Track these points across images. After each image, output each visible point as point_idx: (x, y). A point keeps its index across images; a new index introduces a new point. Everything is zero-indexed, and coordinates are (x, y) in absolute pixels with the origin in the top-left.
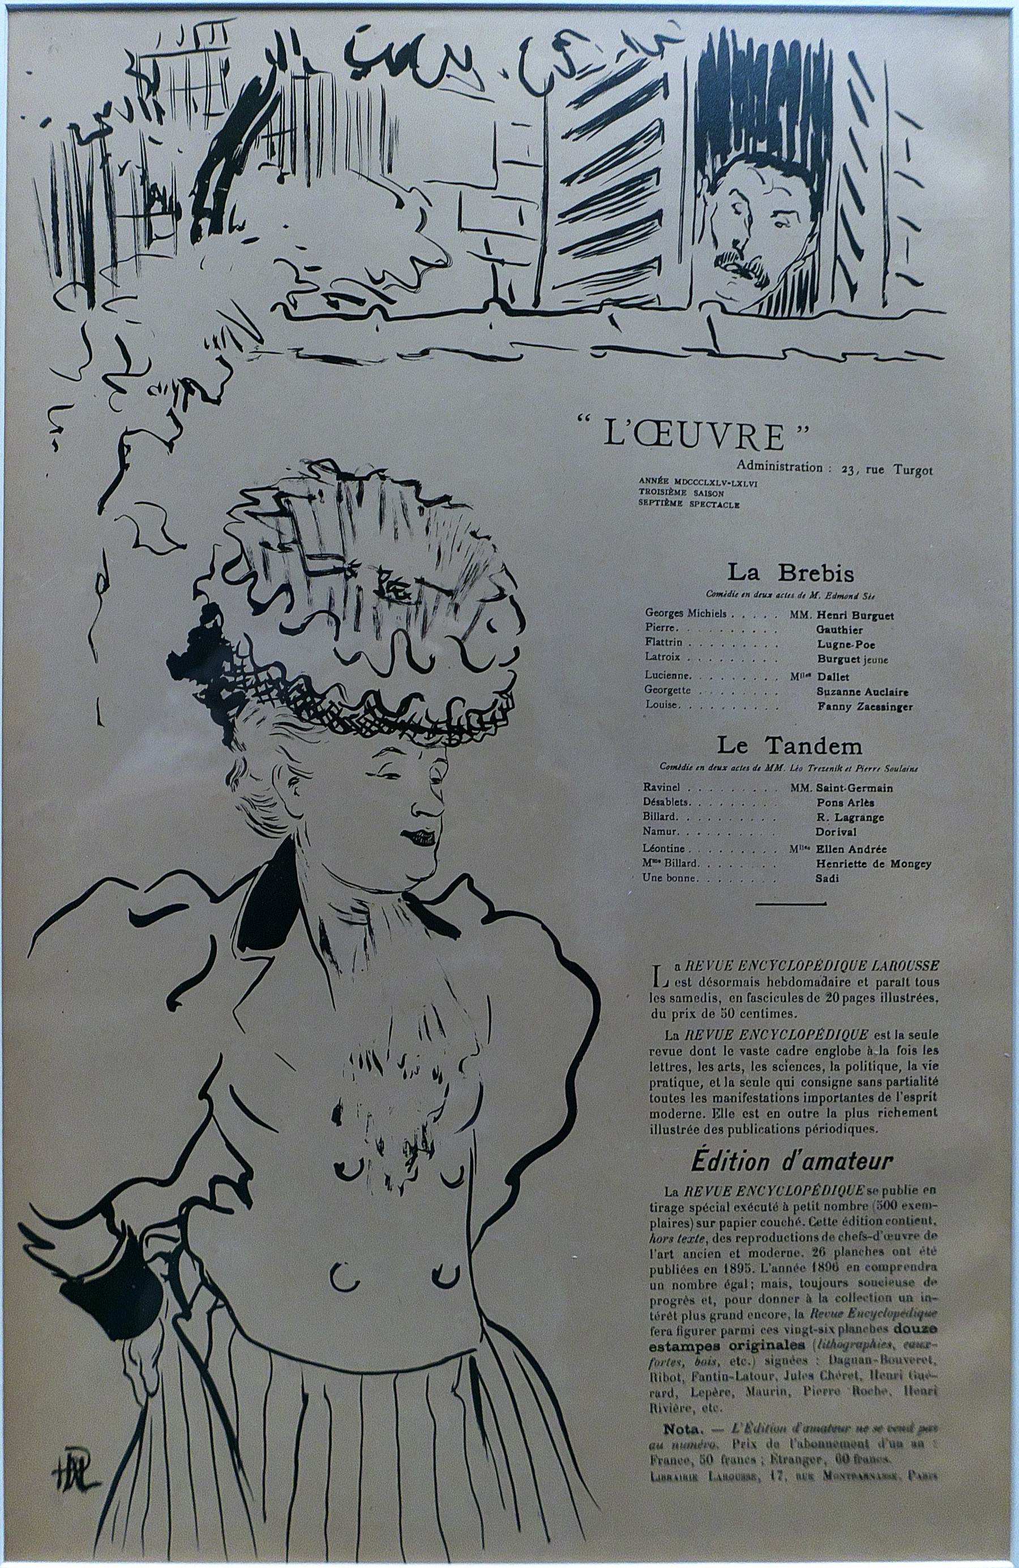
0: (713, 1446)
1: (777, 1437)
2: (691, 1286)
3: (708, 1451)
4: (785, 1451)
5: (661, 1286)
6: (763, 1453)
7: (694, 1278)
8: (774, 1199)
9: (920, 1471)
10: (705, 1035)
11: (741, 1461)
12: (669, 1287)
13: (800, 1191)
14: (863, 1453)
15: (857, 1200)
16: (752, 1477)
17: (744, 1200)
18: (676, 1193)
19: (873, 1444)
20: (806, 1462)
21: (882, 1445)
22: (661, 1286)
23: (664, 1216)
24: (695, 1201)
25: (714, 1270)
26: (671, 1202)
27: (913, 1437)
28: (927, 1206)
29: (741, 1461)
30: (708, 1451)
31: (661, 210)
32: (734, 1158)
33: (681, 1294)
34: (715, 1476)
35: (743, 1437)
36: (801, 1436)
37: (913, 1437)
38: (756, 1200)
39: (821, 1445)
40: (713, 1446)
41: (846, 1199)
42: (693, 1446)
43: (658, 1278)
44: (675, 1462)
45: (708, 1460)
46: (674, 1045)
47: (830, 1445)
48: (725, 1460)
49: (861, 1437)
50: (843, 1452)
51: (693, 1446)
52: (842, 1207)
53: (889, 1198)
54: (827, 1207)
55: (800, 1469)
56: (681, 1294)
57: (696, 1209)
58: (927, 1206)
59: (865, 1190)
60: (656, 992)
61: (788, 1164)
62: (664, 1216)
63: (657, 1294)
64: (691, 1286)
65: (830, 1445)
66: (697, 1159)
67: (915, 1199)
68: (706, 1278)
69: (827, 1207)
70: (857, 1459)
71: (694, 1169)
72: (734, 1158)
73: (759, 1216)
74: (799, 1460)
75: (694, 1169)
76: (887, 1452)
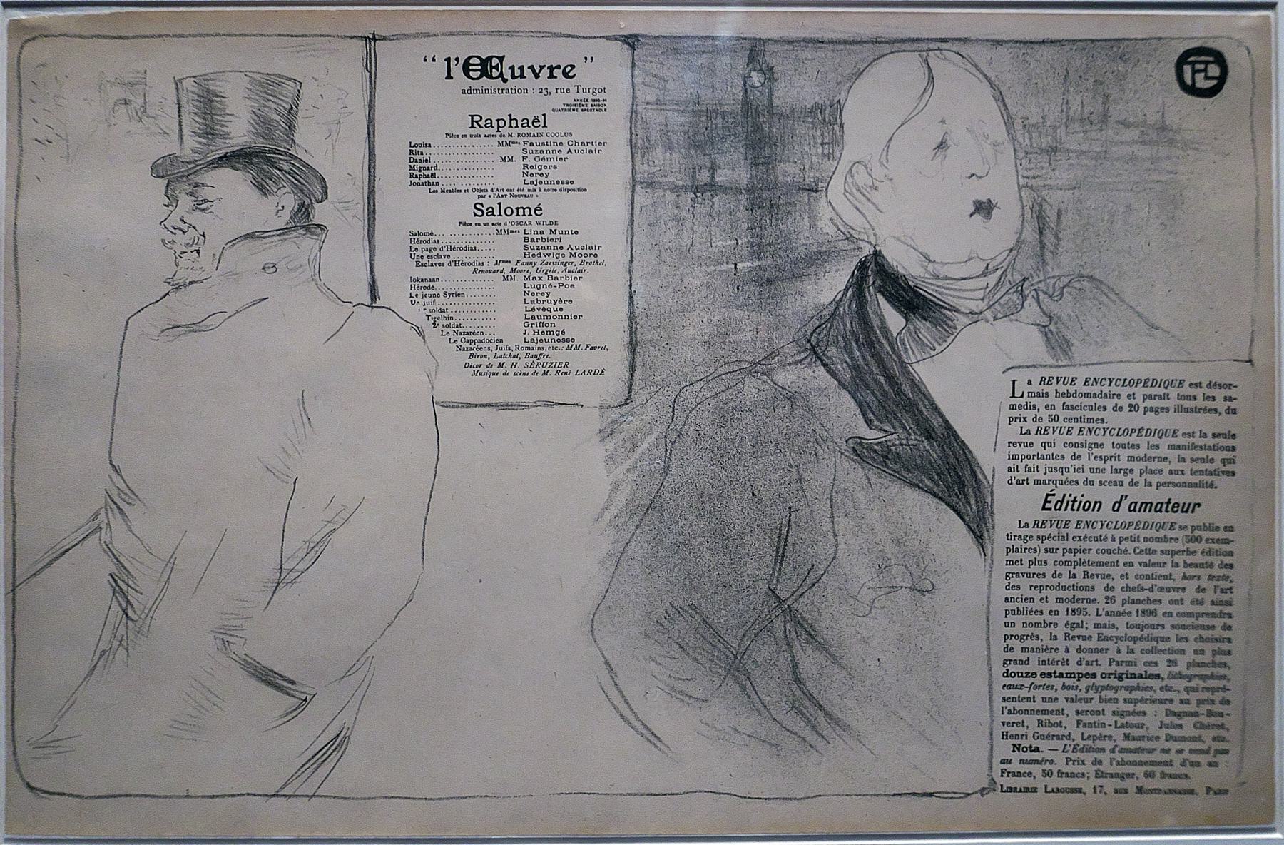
0: (1052, 762)
1: (1100, 756)
2: (1037, 625)
3: (1047, 767)
4: (1105, 767)
5: (1013, 625)
6: (1089, 769)
7: (1039, 619)
8: (1104, 532)
9: (1215, 787)
10: (1048, 524)
11: (1073, 775)
12: (1019, 625)
13: (1127, 525)
14: (1167, 770)
15: (1170, 534)
16: (1079, 791)
17: (1080, 532)
18: (1027, 525)
19: (1177, 763)
20: (1122, 777)
21: (1183, 764)
22: (1013, 625)
23: (1018, 544)
24: (1041, 532)
25: (1057, 613)
26: (1024, 532)
27: (1210, 758)
28: (1227, 541)
29: (1073, 775)
30: (1047, 767)
31: (811, 711)
32: (1074, 501)
33: (1028, 631)
34: (1049, 789)
35: (1074, 756)
36: (1118, 756)
37: (1210, 758)
38: (1090, 532)
39: (1134, 763)
40: (1052, 762)
41: (1161, 534)
42: (1036, 762)
43: (1010, 618)
44: (1019, 775)
45: (1048, 774)
46: (1026, 438)
47: (1141, 763)
48: (1060, 774)
49: (1165, 757)
50: (1150, 768)
51: (1036, 762)
52: (1158, 540)
53: (1197, 533)
54: (1146, 540)
55: (1119, 784)
56: (1028, 631)
57: (1041, 539)
58: (1227, 541)
59: (1177, 526)
60: (1014, 401)
61: (1116, 506)
62: (1018, 544)
63: (1010, 631)
64: (1037, 625)
65: (1141, 763)
66: (1046, 501)
67: (1215, 535)
68: (1049, 619)
69: (1146, 540)
70: (1164, 775)
71: (1044, 508)
72: (1074, 501)
73: (1095, 545)
74: (1117, 775)
75: (1044, 508)
76: (1187, 770)
